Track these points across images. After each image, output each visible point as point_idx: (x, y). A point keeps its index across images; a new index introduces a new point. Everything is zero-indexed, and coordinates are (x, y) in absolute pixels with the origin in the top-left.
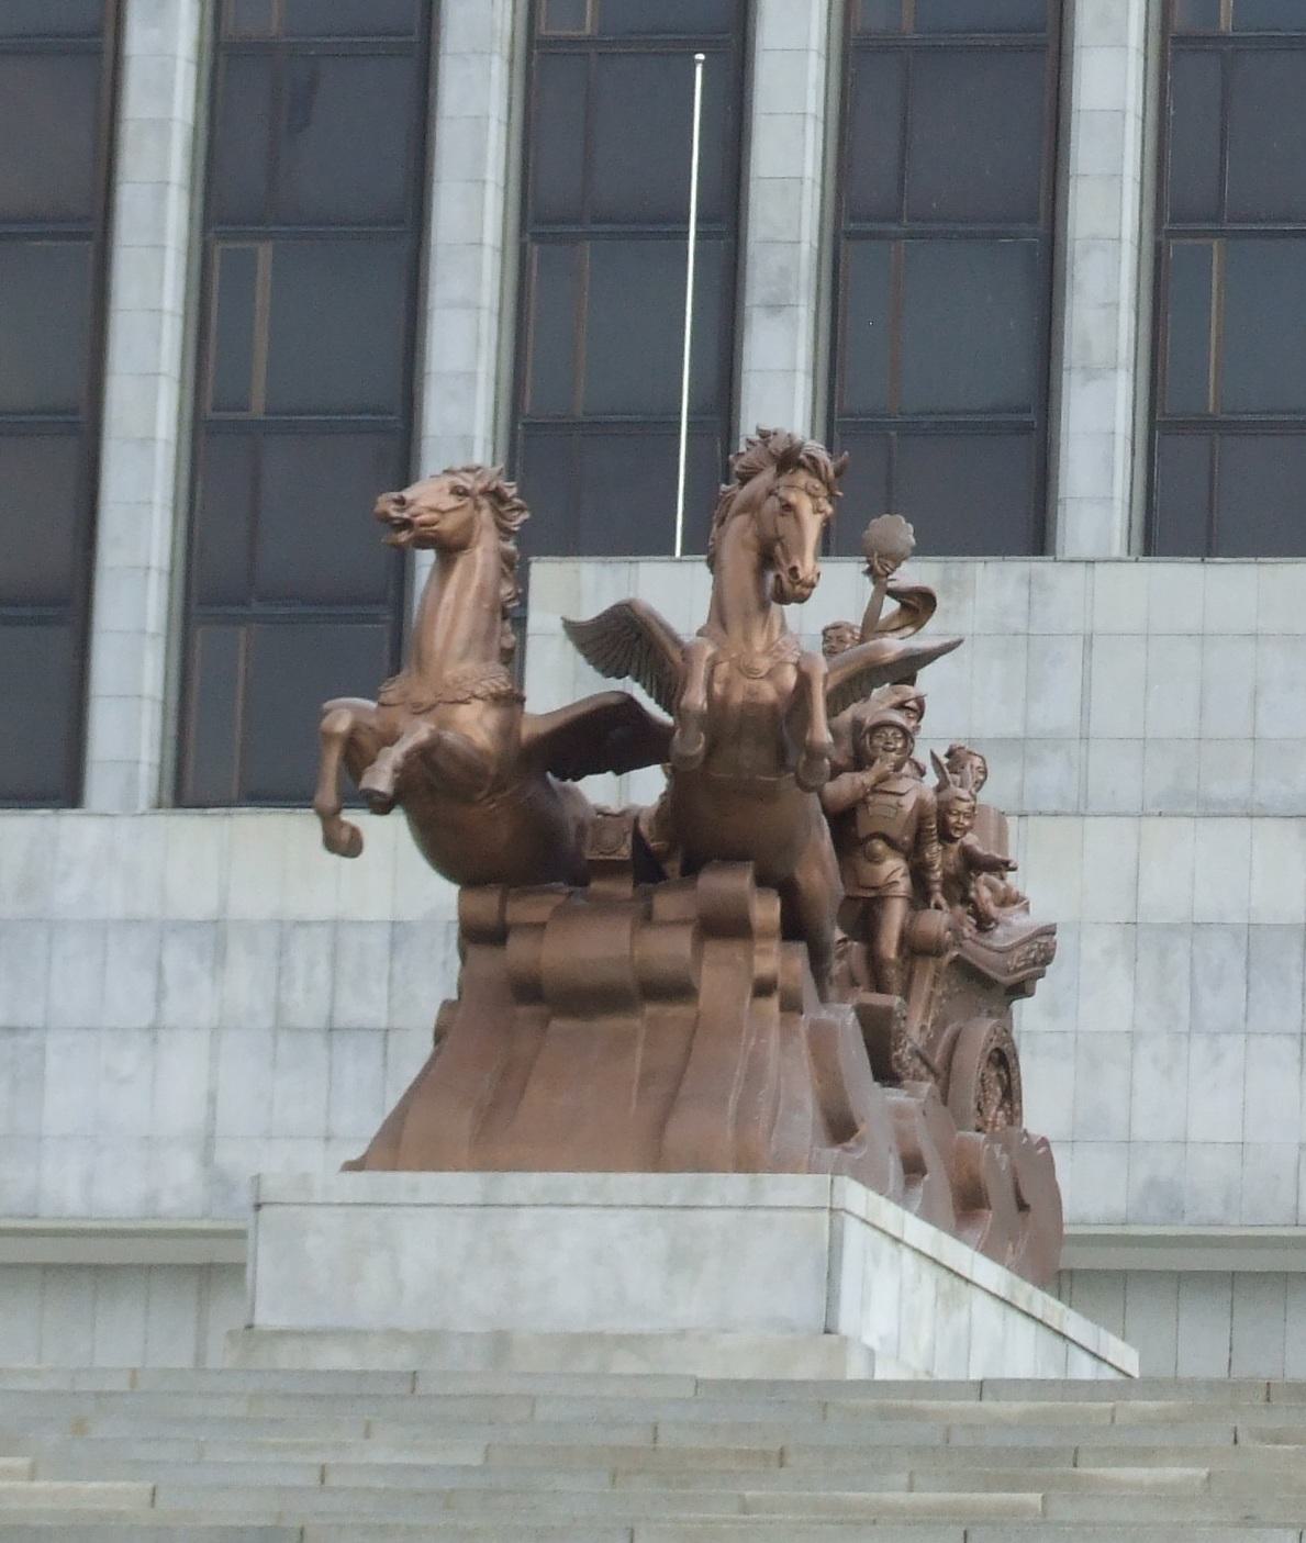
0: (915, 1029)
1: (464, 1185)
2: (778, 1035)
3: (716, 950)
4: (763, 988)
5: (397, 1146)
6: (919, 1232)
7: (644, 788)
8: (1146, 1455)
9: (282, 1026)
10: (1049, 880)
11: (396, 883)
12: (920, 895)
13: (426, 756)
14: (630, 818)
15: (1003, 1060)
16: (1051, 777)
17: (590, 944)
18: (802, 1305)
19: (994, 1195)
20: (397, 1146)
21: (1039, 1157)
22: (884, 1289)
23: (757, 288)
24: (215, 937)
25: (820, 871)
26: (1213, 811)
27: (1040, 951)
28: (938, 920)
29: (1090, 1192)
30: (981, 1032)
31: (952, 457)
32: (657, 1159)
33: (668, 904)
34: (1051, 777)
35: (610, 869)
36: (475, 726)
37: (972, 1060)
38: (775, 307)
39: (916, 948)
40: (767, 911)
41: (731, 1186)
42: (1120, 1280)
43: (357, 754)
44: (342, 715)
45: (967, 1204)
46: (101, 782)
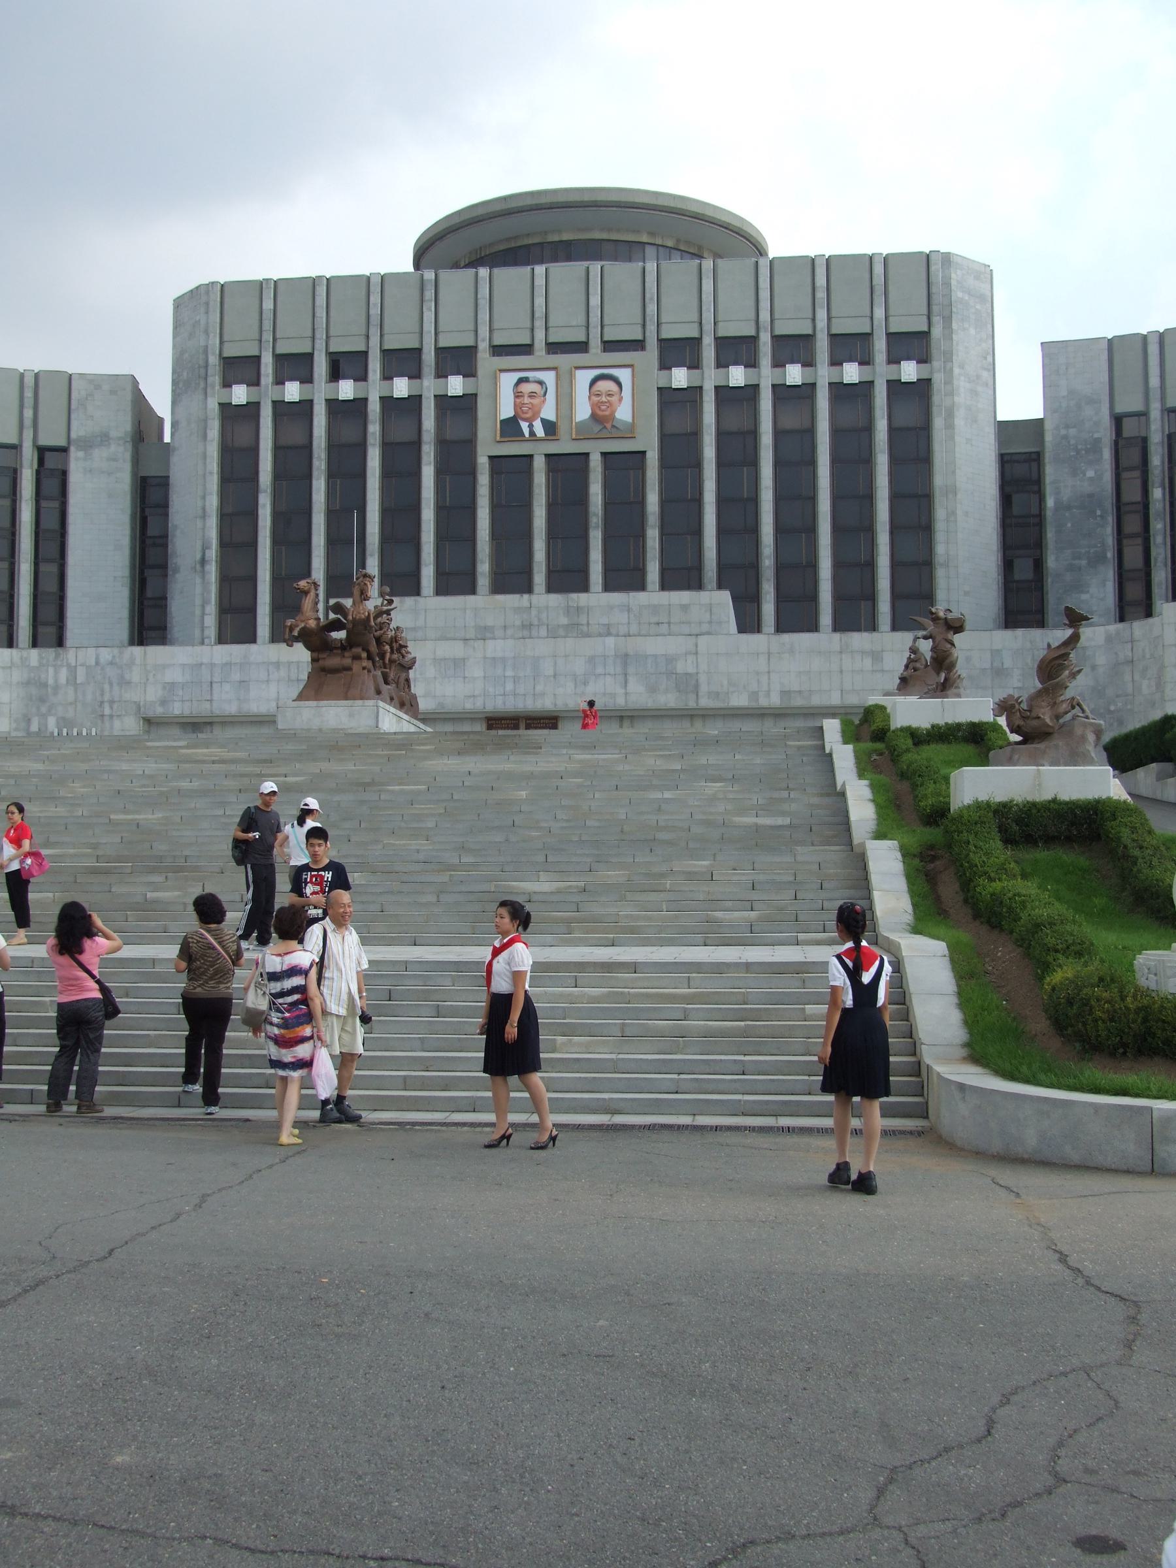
0: (392, 675)
1: (314, 703)
2: (370, 679)
3: (356, 662)
4: (364, 668)
5: (301, 697)
6: (392, 710)
7: (341, 635)
8: (423, 744)
9: (290, 680)
10: (414, 650)
11: (301, 654)
12: (392, 652)
13: (303, 629)
14: (341, 640)
15: (408, 680)
16: (420, 634)
17: (333, 661)
18: (372, 722)
19: (407, 704)
20: (301, 697)
21: (414, 697)
22: (387, 720)
23: (368, 552)
24: (277, 665)
25: (373, 648)
26: (448, 639)
27: (413, 661)
28: (395, 656)
29: (424, 705)
30: (404, 675)
31: (402, 581)
32: (346, 699)
33: (347, 654)
34: (420, 634)
35: (336, 648)
36: (312, 624)
37: (402, 680)
38: (371, 555)
39: (391, 661)
40: (364, 655)
41: (360, 702)
42: (435, 720)
43: (291, 629)
44: (289, 622)
45: (402, 705)
46: (259, 640)
